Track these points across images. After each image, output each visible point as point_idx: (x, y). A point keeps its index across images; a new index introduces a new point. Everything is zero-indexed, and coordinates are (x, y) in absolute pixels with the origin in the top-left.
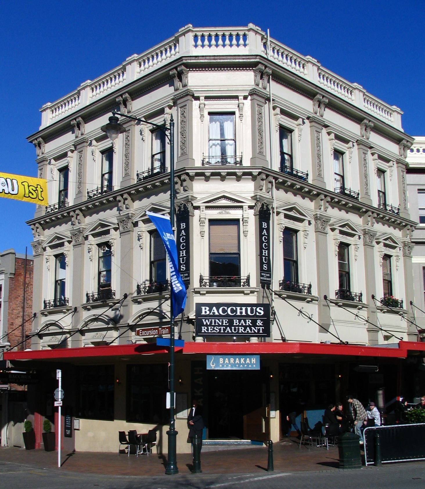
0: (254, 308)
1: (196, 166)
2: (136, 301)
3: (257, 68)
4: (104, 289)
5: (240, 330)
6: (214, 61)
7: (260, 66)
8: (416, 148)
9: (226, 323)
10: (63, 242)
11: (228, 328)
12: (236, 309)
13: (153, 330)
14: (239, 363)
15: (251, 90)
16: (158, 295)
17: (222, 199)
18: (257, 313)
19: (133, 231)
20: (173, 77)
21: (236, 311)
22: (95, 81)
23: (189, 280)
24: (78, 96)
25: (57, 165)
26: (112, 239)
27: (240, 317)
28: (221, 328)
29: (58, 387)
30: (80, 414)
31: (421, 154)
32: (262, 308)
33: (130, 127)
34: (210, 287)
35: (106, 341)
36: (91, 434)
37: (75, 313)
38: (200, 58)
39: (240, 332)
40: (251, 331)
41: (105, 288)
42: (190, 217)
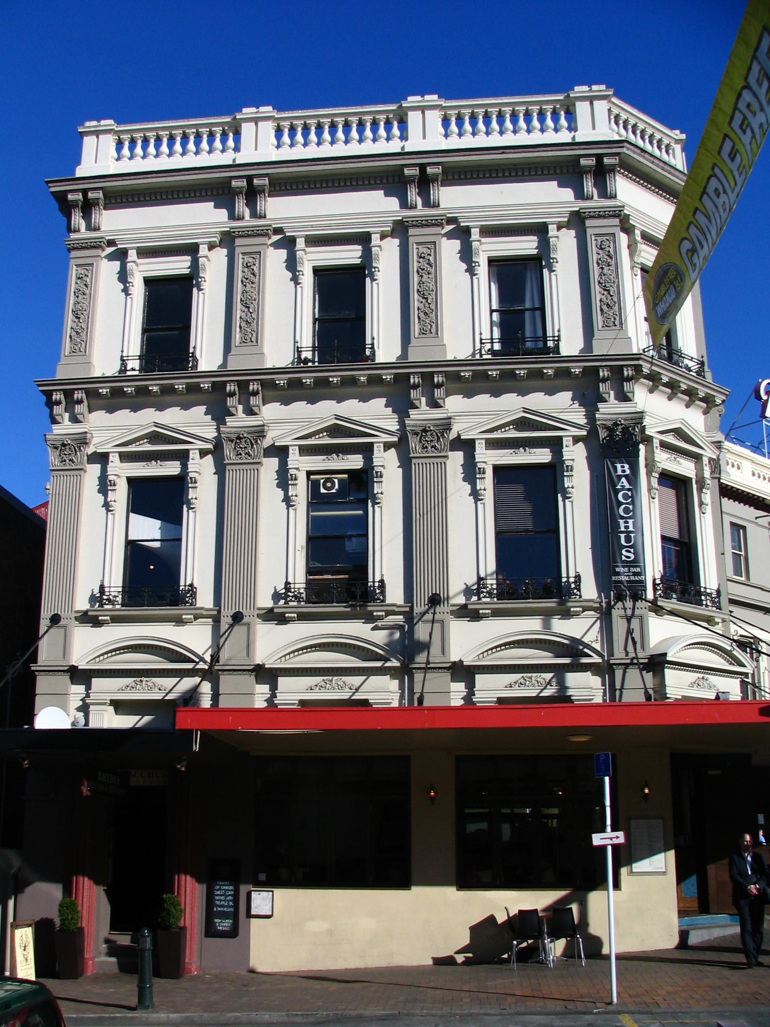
4: (321, 577)
20: (409, 180)
25: (142, 268)
33: (262, 246)
36: (316, 926)
37: (52, 630)
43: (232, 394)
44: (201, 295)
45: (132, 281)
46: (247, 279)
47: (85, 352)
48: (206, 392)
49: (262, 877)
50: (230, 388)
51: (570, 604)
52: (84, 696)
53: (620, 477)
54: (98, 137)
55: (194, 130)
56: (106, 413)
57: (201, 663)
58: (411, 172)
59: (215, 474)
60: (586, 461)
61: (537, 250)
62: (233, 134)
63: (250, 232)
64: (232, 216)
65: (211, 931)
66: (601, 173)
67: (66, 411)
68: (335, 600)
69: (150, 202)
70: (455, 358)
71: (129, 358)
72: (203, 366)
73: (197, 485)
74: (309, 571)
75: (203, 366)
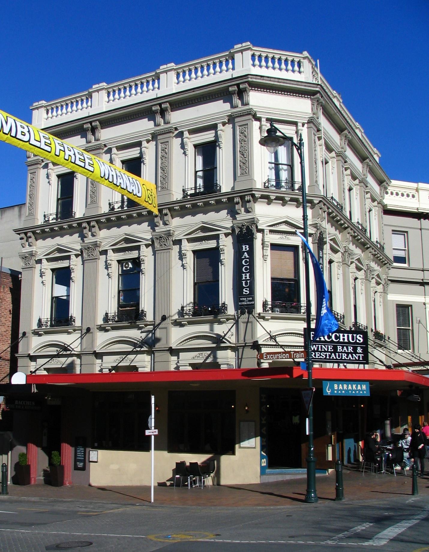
0: (355, 335)
1: (257, 187)
2: (177, 324)
3: (315, 96)
5: (343, 356)
6: (278, 84)
7: (318, 95)
8: (406, 193)
9: (331, 350)
10: (70, 256)
11: (333, 354)
12: (339, 335)
13: (283, 354)
14: (351, 389)
15: (309, 118)
16: (212, 318)
17: (283, 224)
18: (357, 340)
19: (172, 250)
20: (155, 112)
21: (339, 338)
22: (115, 85)
23: (254, 304)
24: (87, 98)
25: (56, 170)
26: (144, 256)
27: (343, 344)
28: (327, 354)
29: (151, 414)
30: (96, 445)
31: (411, 199)
32: (361, 336)
34: (272, 312)
35: (136, 366)
36: (114, 467)
38: (265, 78)
39: (343, 358)
40: (353, 358)
41: (127, 309)
42: (254, 240)
43: (238, 203)
44: (221, 151)
45: (145, 157)
46: (163, 156)
47: (249, 173)
48: (146, 216)
49: (96, 445)
50: (236, 200)
51: (219, 317)
52: (177, 362)
53: (244, 252)
54: (167, 73)
55: (75, 100)
56: (180, 218)
57: (73, 351)
58: (155, 108)
59: (153, 255)
60: (232, 245)
61: (214, 138)
62: (231, 60)
63: (241, 114)
64: (232, 107)
65: (76, 468)
66: (241, 93)
67: (242, 207)
68: (203, 315)
69: (189, 105)
70: (104, 212)
71: (189, 189)
72: (223, 190)
73: (144, 262)
74: (120, 306)
75: (223, 190)
